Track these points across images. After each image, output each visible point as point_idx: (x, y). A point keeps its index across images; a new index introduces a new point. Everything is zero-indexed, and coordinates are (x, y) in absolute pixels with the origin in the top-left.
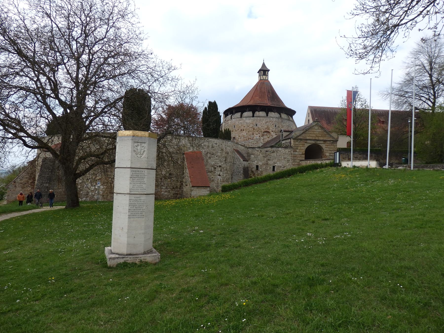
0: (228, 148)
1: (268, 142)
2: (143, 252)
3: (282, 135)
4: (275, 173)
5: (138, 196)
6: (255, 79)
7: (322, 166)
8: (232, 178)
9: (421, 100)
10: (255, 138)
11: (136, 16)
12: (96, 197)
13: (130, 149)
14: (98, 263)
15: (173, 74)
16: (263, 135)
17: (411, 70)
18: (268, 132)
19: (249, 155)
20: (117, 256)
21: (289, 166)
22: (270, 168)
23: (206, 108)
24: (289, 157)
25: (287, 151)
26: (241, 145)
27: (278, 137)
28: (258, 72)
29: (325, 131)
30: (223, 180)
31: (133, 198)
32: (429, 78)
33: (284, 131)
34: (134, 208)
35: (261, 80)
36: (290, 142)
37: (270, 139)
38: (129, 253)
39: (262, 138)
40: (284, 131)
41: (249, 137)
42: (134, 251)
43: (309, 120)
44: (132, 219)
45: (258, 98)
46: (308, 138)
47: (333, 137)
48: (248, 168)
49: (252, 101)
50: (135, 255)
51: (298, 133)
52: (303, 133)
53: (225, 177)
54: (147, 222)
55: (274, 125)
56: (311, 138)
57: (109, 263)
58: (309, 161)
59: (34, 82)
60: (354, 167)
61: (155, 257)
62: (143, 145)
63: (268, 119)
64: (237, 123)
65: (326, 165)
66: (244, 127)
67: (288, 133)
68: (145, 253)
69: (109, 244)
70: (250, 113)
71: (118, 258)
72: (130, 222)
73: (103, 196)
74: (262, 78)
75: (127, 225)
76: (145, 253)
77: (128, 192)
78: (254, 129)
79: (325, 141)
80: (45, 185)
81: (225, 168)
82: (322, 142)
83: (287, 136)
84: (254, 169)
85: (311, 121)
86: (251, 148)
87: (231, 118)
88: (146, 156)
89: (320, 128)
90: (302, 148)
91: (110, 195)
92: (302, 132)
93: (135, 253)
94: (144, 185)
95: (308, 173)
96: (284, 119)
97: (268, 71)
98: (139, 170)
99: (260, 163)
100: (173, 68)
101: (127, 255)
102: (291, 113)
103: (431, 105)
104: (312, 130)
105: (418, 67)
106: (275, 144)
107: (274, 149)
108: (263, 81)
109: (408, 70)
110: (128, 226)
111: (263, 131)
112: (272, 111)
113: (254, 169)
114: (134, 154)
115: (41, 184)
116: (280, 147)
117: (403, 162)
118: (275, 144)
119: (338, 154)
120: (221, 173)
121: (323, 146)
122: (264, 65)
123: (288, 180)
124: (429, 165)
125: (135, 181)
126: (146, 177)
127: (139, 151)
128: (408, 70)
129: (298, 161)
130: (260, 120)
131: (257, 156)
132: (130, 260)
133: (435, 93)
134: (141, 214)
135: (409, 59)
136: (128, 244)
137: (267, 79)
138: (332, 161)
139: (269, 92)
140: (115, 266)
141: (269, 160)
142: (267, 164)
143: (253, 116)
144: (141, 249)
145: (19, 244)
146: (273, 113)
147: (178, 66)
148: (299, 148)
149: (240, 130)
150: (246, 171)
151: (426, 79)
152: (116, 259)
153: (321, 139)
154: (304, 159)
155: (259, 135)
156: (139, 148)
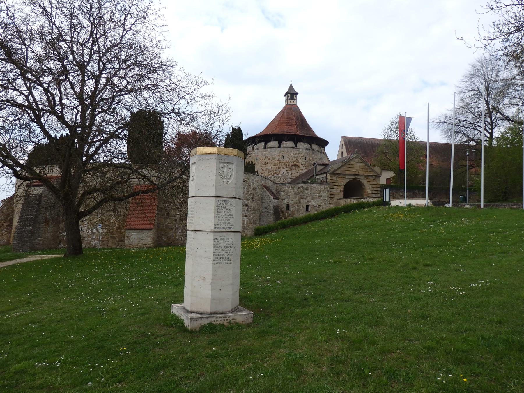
0: (256, 183)
1: (297, 178)
2: (230, 309)
3: (316, 168)
4: (308, 213)
5: (224, 234)
6: (281, 103)
7: (369, 205)
8: (260, 219)
9: (477, 129)
10: (281, 172)
11: (162, 18)
12: (93, 243)
13: (215, 172)
14: (171, 326)
15: (204, 90)
16: (291, 170)
17: (465, 95)
18: (297, 166)
19: (278, 192)
20: (199, 316)
21: (326, 206)
22: (303, 207)
23: (228, 136)
24: (325, 195)
25: (323, 187)
26: (270, 180)
27: (309, 172)
28: (285, 96)
29: (367, 164)
30: (250, 221)
31: (218, 237)
32: (485, 105)
33: (318, 164)
34: (220, 251)
35: (288, 104)
36: (326, 178)
37: (299, 174)
38: (213, 311)
39: (290, 173)
40: (318, 164)
41: (275, 171)
42: (220, 309)
43: (342, 153)
44: (217, 265)
45: (284, 125)
46: (347, 172)
47: (376, 172)
48: (279, 207)
49: (278, 129)
50: (221, 313)
51: (335, 167)
52: (341, 167)
53: (252, 218)
54: (232, 271)
55: (304, 158)
56: (350, 172)
57: (187, 324)
58: (349, 200)
59: (24, 97)
60: (410, 205)
61: (247, 316)
62: (230, 166)
63: (296, 151)
64: (260, 154)
65: (374, 204)
66: (269, 159)
67: (322, 167)
68: (232, 311)
69: (180, 300)
70: (276, 144)
71: (201, 318)
72: (214, 270)
73: (103, 241)
74: (289, 103)
75: (211, 273)
76: (232, 311)
77: (212, 228)
78: (280, 162)
79: (366, 176)
80: (28, 228)
81: (252, 208)
82: (363, 178)
83: (322, 170)
84: (284, 209)
85: (345, 155)
86: (281, 184)
87: (253, 149)
88: (235, 181)
89: (360, 161)
90: (340, 184)
91: (111, 241)
92: (340, 165)
93: (221, 311)
94: (231, 219)
95: (354, 213)
96: (315, 150)
97: (297, 94)
98: (225, 199)
99: (291, 202)
100: (203, 83)
101: (211, 314)
102: (323, 143)
103: (489, 136)
104: (352, 163)
105: (472, 93)
106: (308, 179)
107: (307, 185)
108: (290, 106)
109: (462, 95)
110: (213, 274)
111: (291, 164)
112: (301, 141)
113: (284, 209)
114: (219, 178)
115: (23, 228)
116: (313, 182)
117: (462, 200)
118: (308, 179)
119: (387, 190)
120: (248, 214)
121: (365, 182)
122: (291, 87)
123: (322, 223)
124: (492, 204)
125: (221, 214)
126: (234, 208)
127: (225, 174)
128: (462, 95)
129: (336, 199)
130: (288, 151)
131: (288, 193)
132: (216, 320)
133: (492, 121)
134: (228, 258)
135: (463, 83)
136: (213, 299)
137: (295, 103)
138: (380, 199)
139: (297, 119)
140: (198, 329)
141: (301, 198)
142: (300, 203)
143: (279, 147)
144: (228, 306)
145: (29, 303)
146: (303, 144)
147: (210, 81)
148: (337, 184)
149: (263, 163)
150: (277, 211)
151: (482, 107)
152: (200, 320)
153: (362, 173)
154: (342, 197)
155: (286, 169)
156: (225, 170)
